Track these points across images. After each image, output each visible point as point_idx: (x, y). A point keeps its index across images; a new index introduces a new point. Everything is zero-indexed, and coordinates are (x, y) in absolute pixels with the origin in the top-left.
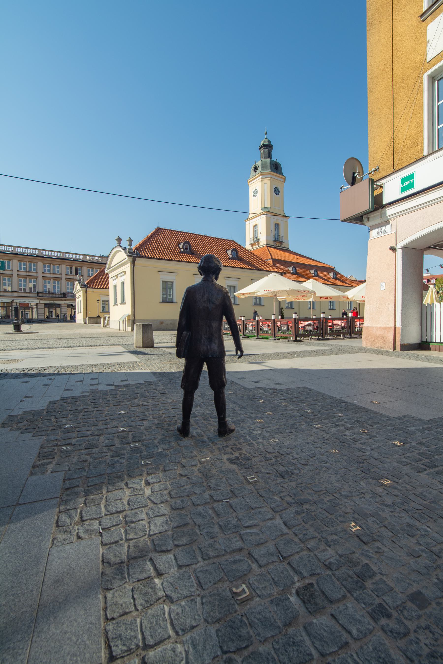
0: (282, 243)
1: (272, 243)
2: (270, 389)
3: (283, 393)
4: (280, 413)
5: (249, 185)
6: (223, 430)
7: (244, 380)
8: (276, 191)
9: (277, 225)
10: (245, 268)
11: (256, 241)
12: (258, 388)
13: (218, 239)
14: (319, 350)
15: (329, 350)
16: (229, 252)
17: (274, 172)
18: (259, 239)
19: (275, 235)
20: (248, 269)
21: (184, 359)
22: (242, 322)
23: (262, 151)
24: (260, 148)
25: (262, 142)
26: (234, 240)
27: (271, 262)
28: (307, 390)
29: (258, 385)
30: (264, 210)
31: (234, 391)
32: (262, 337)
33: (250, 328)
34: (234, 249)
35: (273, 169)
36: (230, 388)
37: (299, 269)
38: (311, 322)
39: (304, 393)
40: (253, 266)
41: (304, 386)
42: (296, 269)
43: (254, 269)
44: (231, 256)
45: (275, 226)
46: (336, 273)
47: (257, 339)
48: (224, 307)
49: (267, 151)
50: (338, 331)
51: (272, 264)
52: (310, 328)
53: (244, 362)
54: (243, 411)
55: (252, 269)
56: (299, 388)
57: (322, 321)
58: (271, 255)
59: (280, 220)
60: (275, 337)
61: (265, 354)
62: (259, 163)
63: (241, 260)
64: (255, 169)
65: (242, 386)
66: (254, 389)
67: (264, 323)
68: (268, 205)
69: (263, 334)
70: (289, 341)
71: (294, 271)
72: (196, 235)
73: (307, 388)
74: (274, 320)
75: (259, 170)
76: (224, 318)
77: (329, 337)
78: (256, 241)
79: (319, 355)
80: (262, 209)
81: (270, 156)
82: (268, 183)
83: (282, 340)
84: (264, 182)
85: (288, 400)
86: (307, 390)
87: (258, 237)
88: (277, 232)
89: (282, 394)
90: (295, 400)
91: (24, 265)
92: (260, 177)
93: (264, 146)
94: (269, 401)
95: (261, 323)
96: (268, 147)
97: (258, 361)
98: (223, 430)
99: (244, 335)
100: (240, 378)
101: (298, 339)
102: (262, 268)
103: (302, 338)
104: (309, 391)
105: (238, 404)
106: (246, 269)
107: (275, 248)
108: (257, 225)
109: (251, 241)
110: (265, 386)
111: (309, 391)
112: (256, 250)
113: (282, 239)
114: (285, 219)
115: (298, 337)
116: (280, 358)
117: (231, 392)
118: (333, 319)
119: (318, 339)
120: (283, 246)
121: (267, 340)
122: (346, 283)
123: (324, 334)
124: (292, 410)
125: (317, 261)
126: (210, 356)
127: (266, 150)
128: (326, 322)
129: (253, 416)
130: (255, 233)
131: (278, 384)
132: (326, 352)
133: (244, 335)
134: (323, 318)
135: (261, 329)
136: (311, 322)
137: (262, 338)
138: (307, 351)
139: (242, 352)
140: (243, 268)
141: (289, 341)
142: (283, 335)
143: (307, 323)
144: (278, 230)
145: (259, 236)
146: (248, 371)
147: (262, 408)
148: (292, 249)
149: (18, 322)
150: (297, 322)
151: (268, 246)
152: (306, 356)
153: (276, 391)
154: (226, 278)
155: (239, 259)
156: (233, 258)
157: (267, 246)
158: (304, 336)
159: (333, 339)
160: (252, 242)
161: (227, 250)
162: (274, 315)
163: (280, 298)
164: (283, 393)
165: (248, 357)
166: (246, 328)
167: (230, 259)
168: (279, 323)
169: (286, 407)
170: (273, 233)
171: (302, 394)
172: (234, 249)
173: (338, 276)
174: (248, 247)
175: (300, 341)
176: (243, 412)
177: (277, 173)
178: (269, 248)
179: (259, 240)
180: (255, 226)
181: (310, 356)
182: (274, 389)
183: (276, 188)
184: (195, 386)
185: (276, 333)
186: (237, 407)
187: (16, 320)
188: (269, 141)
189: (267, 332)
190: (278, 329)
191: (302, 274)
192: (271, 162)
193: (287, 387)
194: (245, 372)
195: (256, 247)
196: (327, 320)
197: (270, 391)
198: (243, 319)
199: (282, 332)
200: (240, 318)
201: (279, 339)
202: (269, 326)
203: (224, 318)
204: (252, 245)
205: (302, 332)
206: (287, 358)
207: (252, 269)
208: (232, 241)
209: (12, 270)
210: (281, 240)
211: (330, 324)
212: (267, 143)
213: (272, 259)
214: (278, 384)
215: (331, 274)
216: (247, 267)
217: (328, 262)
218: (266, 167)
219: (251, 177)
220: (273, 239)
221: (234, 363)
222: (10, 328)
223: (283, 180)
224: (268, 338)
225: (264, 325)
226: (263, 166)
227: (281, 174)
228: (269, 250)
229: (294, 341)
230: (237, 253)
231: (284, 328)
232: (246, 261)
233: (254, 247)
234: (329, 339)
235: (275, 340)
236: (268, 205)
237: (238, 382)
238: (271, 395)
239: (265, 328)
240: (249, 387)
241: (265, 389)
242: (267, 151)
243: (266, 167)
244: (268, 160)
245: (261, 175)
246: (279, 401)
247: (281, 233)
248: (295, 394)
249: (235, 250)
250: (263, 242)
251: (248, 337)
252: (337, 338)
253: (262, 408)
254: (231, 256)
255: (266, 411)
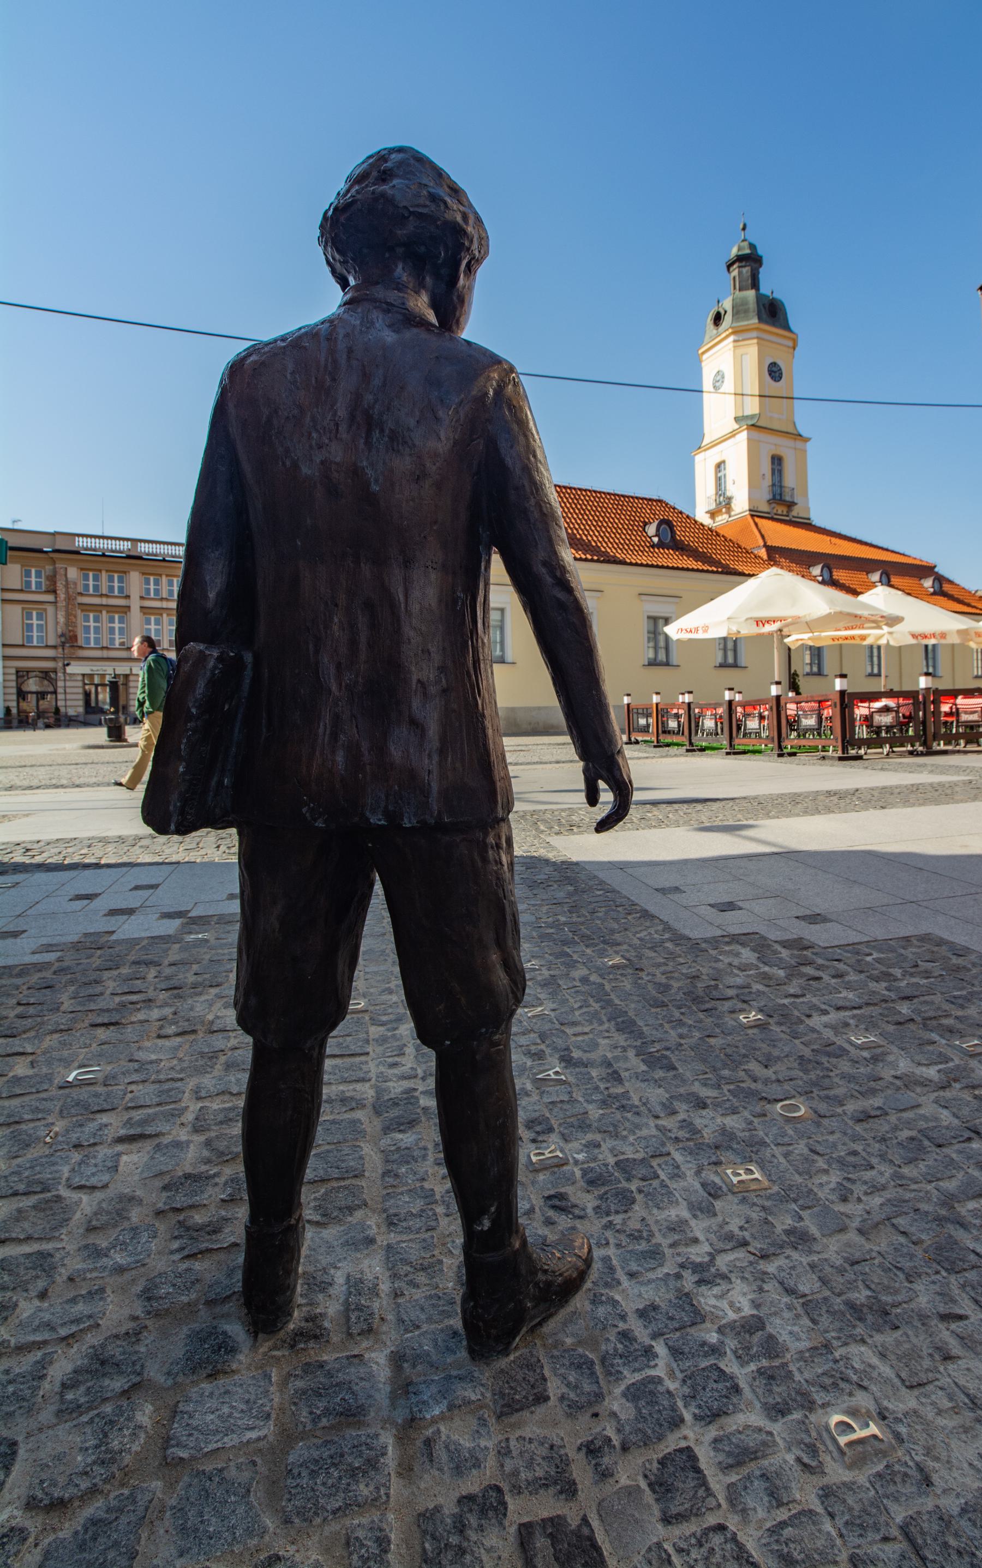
0: (791, 505)
1: (764, 507)
2: (786, 944)
3: (841, 966)
4: (851, 1107)
5: (700, 362)
6: (507, 1294)
7: (676, 897)
8: (774, 372)
9: (777, 461)
10: (693, 570)
11: (724, 504)
12: (735, 939)
13: (624, 496)
14: (931, 785)
15: (964, 783)
16: (651, 530)
17: (766, 323)
18: (730, 499)
19: (773, 485)
20: (702, 571)
21: (234, 831)
22: (686, 707)
23: (735, 273)
24: (729, 267)
25: (734, 251)
26: (663, 498)
27: (763, 553)
28: (944, 951)
29: (734, 923)
30: (743, 423)
31: (632, 954)
32: (742, 748)
33: (709, 723)
34: (663, 522)
35: (764, 316)
36: (617, 937)
37: (844, 568)
38: (891, 703)
39: (936, 969)
40: (717, 563)
41: (925, 927)
42: (831, 573)
43: (717, 572)
44: (656, 540)
45: (773, 463)
46: (940, 579)
47: (728, 754)
48: (498, 503)
49: (746, 271)
50: (972, 728)
51: (765, 557)
52: (887, 719)
53: (685, 823)
54: (658, 1083)
55: (712, 572)
56: (907, 939)
57: (924, 697)
58: (763, 537)
59: (785, 448)
60: (780, 747)
61: (755, 798)
62: (727, 304)
63: (682, 549)
64: (718, 319)
65: (667, 927)
66: (715, 942)
67: (749, 710)
68: (752, 407)
69: (745, 741)
70: (824, 758)
71: (826, 576)
72: (565, 487)
73: (941, 942)
74: (778, 698)
75: (727, 320)
76: (497, 568)
77: (942, 747)
78: (724, 504)
79: (936, 802)
80: (737, 419)
81: (755, 284)
82: (751, 351)
83: (802, 757)
84: (740, 351)
85: (875, 1011)
86: (944, 951)
87: (728, 494)
88: (777, 479)
89: (839, 975)
90: (905, 1009)
91: (156, 583)
92: (732, 338)
93: (741, 259)
94: (785, 1016)
95: (739, 709)
96: (750, 261)
97: (731, 823)
98: (507, 1294)
99: (691, 744)
100: (662, 891)
101: (853, 752)
102: (740, 568)
103: (862, 752)
104: (955, 960)
105: (641, 1035)
106: (698, 570)
107: (772, 519)
108: (724, 462)
109: (709, 504)
110: (762, 930)
111: (955, 960)
112: (723, 526)
113: (792, 496)
114: (799, 444)
115: (850, 747)
116: (806, 812)
117: (617, 960)
118: (954, 694)
119: (911, 753)
120: (794, 513)
121: (757, 756)
122: (969, 605)
123: (930, 737)
124: (908, 1082)
125: (887, 550)
126: (377, 819)
127: (745, 270)
128: (937, 703)
129: (709, 1123)
130: (720, 482)
131: (814, 919)
132: (957, 789)
133: (691, 744)
134: (927, 689)
135: (739, 728)
136: (891, 703)
137: (744, 753)
138: (891, 787)
139: (623, 790)
140: (688, 569)
141: (824, 758)
142: (803, 742)
143: (877, 705)
144: (780, 472)
145: (731, 490)
146: (698, 860)
147: (753, 1066)
148: (817, 521)
149: (117, 718)
150: (846, 701)
151: (755, 514)
152: (893, 806)
153: (807, 953)
154: (644, 597)
155: (679, 547)
156: (661, 545)
157: (752, 516)
158: (869, 743)
159: (959, 752)
160: (713, 506)
161: (645, 524)
162: (778, 683)
163: (793, 640)
164: (841, 966)
165: (699, 807)
166: (697, 726)
167: (653, 546)
168: (791, 709)
169: (875, 1059)
170: (768, 481)
171: (927, 974)
172: (663, 522)
173: (946, 587)
174: (702, 516)
175: (859, 758)
176: (656, 1095)
177: (774, 325)
178: (757, 520)
179: (729, 500)
180: (720, 466)
181: (906, 803)
182: (798, 944)
183: (773, 364)
184: (330, 1006)
185: (784, 735)
186: (631, 1053)
187: (112, 713)
188: (752, 246)
189: (758, 734)
190: (791, 725)
191: (847, 583)
192: (760, 298)
193: (854, 937)
194: (686, 862)
195: (722, 519)
196: (939, 695)
197: (785, 953)
198: (687, 698)
199: (802, 733)
200: (681, 698)
201: (794, 754)
202: (762, 718)
203: (497, 568)
204: (713, 514)
205: (862, 732)
206: (829, 810)
207: (712, 572)
208: (660, 501)
209: (128, 597)
210: (788, 498)
211: (945, 708)
212: (747, 251)
213: (765, 546)
214: (814, 919)
215: (928, 583)
216: (700, 566)
217: (919, 552)
218: (746, 311)
219: (707, 338)
220: (768, 496)
221: (651, 827)
222: (100, 734)
223: (790, 344)
224: (759, 752)
225: (746, 715)
226: (739, 311)
227: (787, 327)
228: (756, 524)
229: (840, 759)
230: (673, 533)
231: (810, 722)
232: (696, 550)
233: (719, 518)
234: (945, 752)
235: (780, 755)
236: (752, 407)
237: (652, 909)
238: (789, 977)
239: (753, 724)
240: (695, 934)
241: (761, 945)
242: (746, 271)
243: (746, 311)
244: (751, 294)
245: (733, 333)
246: (833, 1017)
247: (789, 480)
248: (897, 972)
249: (666, 523)
250: (741, 505)
251: (702, 750)
252: (969, 748)
253: (753, 1066)
254: (656, 540)
255: (774, 1090)
